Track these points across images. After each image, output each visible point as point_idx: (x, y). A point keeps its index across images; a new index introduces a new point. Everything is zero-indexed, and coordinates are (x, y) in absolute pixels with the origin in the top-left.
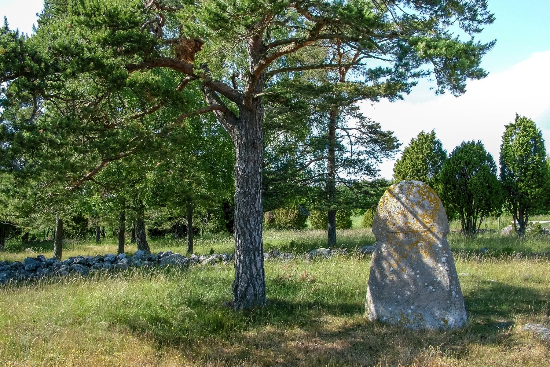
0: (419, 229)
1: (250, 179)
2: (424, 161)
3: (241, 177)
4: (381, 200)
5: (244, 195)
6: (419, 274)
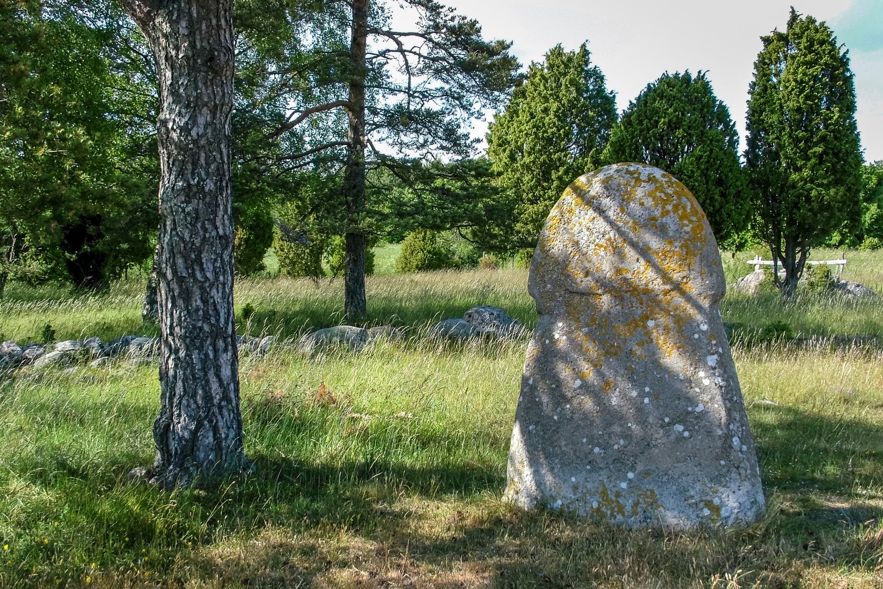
0: (651, 286)
1: (203, 155)
2: (561, 116)
3: (180, 147)
4: (554, 212)
5: (187, 196)
6: (648, 395)
